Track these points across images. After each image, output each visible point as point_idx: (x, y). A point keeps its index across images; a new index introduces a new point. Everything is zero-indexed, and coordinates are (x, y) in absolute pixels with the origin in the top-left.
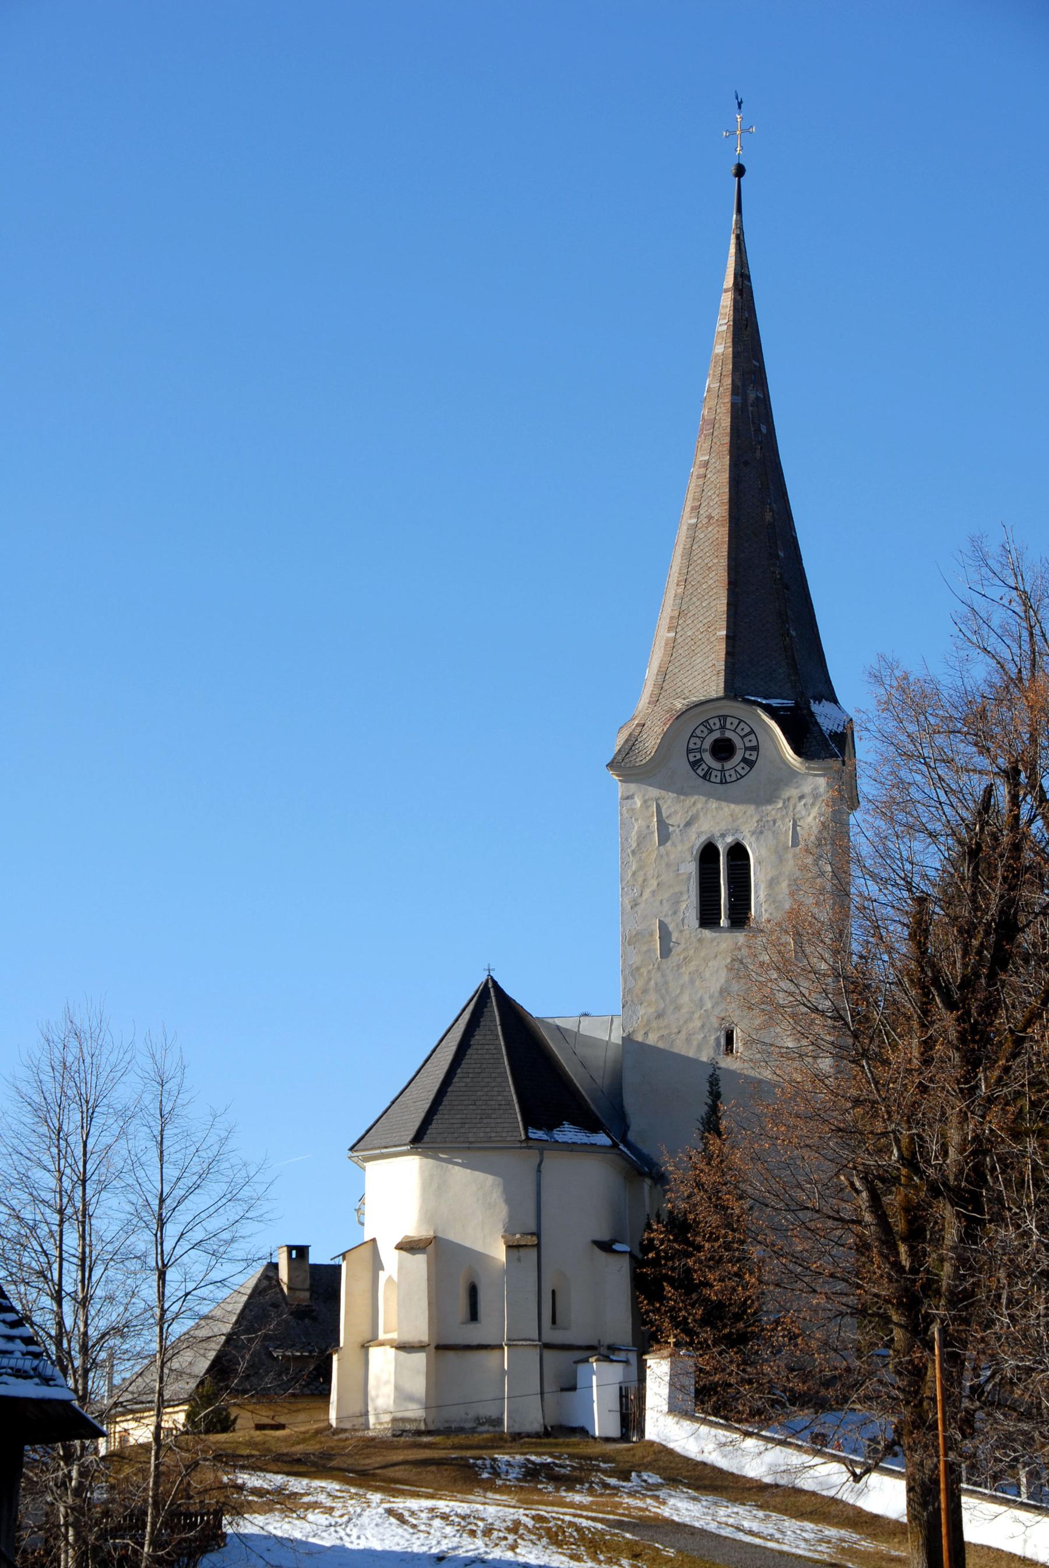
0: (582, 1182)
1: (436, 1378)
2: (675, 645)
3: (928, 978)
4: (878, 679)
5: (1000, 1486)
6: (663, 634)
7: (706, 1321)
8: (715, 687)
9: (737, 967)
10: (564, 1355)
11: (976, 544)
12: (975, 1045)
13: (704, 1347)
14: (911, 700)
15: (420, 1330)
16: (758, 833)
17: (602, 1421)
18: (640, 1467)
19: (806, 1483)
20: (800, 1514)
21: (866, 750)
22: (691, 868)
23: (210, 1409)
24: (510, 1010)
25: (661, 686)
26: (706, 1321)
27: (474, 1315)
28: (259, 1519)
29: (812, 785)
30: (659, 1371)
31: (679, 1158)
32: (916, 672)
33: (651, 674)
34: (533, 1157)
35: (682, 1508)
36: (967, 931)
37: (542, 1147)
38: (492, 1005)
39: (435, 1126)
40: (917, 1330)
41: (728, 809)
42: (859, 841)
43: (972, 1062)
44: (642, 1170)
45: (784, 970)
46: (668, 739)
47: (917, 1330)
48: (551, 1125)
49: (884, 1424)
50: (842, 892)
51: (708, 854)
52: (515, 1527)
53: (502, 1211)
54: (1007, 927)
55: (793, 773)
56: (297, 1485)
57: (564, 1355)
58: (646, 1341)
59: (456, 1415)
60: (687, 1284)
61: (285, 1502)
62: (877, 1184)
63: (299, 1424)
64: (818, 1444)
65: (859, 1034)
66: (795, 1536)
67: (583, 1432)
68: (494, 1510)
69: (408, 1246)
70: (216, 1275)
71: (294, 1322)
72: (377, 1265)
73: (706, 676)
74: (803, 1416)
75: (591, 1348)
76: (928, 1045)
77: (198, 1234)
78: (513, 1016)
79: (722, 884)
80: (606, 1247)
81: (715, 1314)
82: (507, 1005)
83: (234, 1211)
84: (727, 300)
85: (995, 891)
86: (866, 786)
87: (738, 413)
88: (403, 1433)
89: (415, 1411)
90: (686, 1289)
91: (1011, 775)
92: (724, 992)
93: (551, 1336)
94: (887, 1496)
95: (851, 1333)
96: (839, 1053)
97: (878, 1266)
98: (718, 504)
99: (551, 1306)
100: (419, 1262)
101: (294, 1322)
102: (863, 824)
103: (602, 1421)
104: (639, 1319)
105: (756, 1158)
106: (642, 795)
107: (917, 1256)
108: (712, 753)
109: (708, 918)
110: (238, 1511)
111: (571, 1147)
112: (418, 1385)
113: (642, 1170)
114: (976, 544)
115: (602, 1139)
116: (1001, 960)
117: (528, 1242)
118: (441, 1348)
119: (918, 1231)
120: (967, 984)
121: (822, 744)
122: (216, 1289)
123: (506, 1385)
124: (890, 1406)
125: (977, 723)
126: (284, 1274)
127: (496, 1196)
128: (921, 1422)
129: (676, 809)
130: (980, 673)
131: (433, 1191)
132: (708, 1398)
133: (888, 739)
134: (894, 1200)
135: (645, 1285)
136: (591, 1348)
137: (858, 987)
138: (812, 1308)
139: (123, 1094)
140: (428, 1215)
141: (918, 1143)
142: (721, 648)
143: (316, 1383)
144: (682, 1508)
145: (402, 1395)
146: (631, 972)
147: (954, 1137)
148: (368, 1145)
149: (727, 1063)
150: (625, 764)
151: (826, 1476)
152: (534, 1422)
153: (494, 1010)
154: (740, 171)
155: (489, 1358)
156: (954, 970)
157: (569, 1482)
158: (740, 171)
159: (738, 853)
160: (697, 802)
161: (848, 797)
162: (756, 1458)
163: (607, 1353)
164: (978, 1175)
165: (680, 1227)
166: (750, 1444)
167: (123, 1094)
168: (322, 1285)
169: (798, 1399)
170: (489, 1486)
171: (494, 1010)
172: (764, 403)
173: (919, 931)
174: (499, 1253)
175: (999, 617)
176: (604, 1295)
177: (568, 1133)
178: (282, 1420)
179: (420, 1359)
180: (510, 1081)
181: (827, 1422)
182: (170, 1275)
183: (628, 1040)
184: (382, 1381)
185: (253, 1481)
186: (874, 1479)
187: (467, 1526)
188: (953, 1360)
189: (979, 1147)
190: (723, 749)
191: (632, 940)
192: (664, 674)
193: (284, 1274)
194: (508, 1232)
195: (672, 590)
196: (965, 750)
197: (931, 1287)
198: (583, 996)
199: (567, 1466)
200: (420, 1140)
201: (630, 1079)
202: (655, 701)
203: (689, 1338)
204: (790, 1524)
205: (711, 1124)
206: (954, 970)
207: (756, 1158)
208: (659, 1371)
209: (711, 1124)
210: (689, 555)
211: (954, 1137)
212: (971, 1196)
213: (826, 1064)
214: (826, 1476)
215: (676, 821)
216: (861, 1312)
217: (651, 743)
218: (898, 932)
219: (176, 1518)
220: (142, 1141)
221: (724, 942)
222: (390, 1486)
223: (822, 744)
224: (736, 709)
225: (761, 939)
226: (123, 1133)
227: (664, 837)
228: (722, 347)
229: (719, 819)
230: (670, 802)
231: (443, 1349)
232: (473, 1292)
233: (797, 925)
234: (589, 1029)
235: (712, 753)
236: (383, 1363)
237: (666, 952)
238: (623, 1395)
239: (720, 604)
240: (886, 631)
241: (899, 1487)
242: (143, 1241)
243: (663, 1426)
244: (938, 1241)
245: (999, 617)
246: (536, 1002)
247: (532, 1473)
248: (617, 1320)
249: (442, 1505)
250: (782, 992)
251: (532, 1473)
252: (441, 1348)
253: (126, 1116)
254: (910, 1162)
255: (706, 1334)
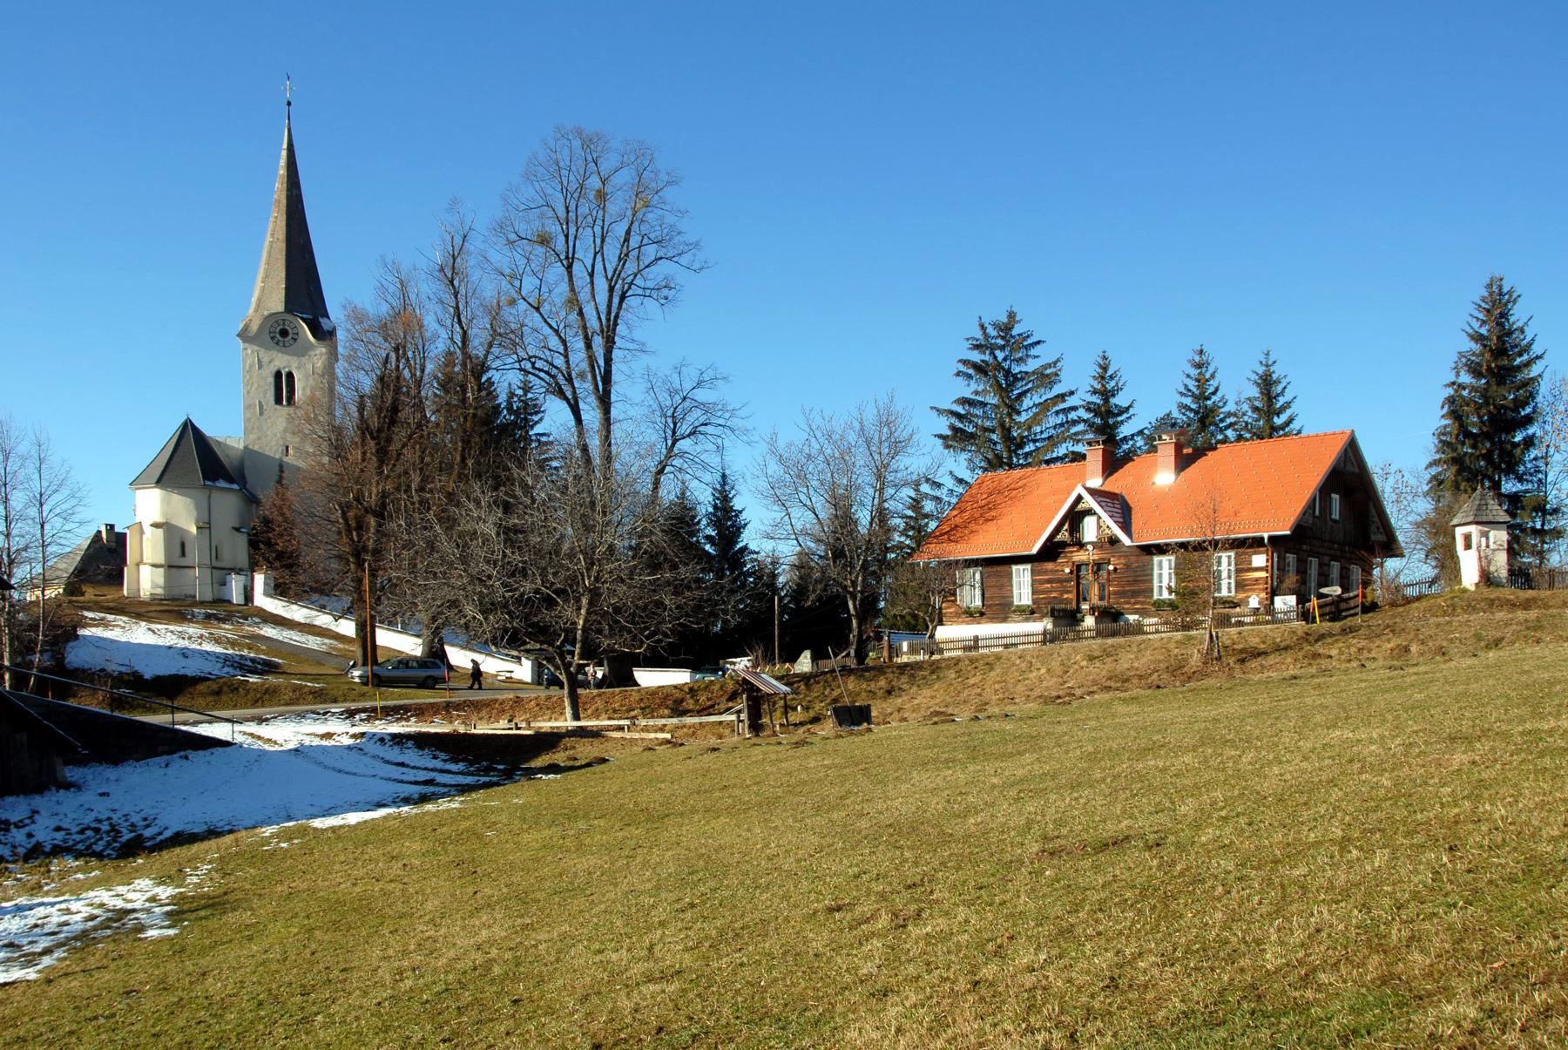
0: (227, 504)
1: (167, 578)
2: (264, 290)
3: (364, 427)
4: (344, 307)
5: (390, 624)
6: (259, 284)
7: (277, 559)
8: (281, 307)
9: (290, 419)
10: (221, 572)
11: (383, 257)
12: (382, 454)
13: (276, 569)
14: (358, 317)
15: (161, 559)
16: (298, 368)
17: (236, 597)
18: (252, 616)
19: (317, 623)
20: (314, 634)
21: (341, 335)
22: (271, 380)
23: (73, 588)
24: (198, 433)
25: (258, 305)
26: (277, 559)
27: (183, 554)
28: (94, 630)
29: (320, 351)
30: (259, 580)
31: (267, 495)
32: (360, 305)
33: (254, 299)
34: (207, 492)
35: (269, 631)
36: (379, 410)
37: (210, 488)
38: (189, 429)
39: (167, 475)
40: (360, 564)
41: (286, 357)
42: (339, 374)
43: (381, 462)
44: (251, 500)
45: (308, 420)
46: (261, 327)
47: (360, 564)
48: (214, 480)
49: (346, 601)
50: (332, 390)
51: (278, 375)
52: (201, 637)
53: (195, 513)
54: (395, 409)
55: (312, 347)
56: (110, 617)
57: (221, 572)
58: (253, 567)
59: (177, 592)
60: (269, 544)
61: (105, 624)
62: (345, 509)
63: (110, 595)
64: (322, 608)
65: (338, 450)
66: (313, 643)
67: (229, 602)
68: (192, 630)
69: (156, 525)
70: (67, 528)
71: (106, 558)
72: (142, 532)
73: (277, 303)
74: (315, 597)
75: (232, 570)
76: (364, 453)
77: (58, 511)
78: (199, 436)
79: (283, 386)
80: (237, 530)
81: (280, 556)
82: (196, 430)
83: (73, 502)
84: (284, 153)
85: (389, 397)
86: (340, 349)
87: (289, 198)
88: (155, 599)
89: (160, 591)
90: (271, 548)
91: (396, 349)
92: (285, 430)
93: (215, 564)
94: (348, 628)
95: (334, 565)
96: (330, 455)
97: (345, 540)
98: (281, 233)
99: (216, 553)
100: (160, 532)
101: (106, 558)
102: (340, 368)
103: (236, 597)
104: (251, 557)
105: (297, 495)
106: (251, 349)
107: (360, 536)
108: (278, 334)
109: (278, 401)
110: (85, 626)
111: (223, 489)
112: (161, 581)
113: (251, 500)
114: (383, 257)
115: (235, 486)
116: (393, 422)
117: (205, 526)
118: (170, 567)
119: (361, 526)
120: (380, 430)
121: (324, 334)
122: (74, 540)
123: (198, 583)
124: (349, 593)
125: (384, 328)
126: (104, 535)
127: (192, 507)
128: (361, 600)
129: (266, 356)
130: (384, 309)
131: (166, 503)
132: (279, 590)
133: (348, 331)
134: (351, 514)
135: (253, 544)
136: (232, 570)
137: (338, 431)
138: (319, 556)
139: (23, 448)
140: (164, 514)
141: (360, 492)
142: (283, 292)
143: (116, 578)
144: (269, 631)
145: (155, 586)
146: (247, 420)
147: (374, 491)
148: (137, 483)
149: (286, 459)
150: (244, 335)
151: (324, 620)
152: (209, 597)
153: (189, 431)
154: (289, 104)
155: (190, 572)
156: (375, 423)
157: (224, 621)
158: (289, 104)
159: (290, 376)
160: (274, 353)
161: (333, 355)
162: (298, 613)
163: (239, 571)
164: (384, 506)
165: (267, 522)
166: (294, 607)
167: (23, 448)
168: (120, 539)
169: (314, 590)
170: (190, 621)
171: (189, 431)
172: (300, 196)
173: (361, 407)
174: (194, 530)
175: (392, 289)
176: (236, 550)
177: (222, 484)
178: (216, 814)
179: (161, 570)
180: (195, 460)
181: (324, 600)
182: (47, 527)
183: (246, 447)
184: (146, 579)
185: (90, 615)
186: (342, 621)
187: (181, 635)
188: (373, 575)
189: (384, 495)
190: (284, 333)
191: (248, 407)
192: (259, 300)
193: (104, 535)
194: (197, 522)
195: (263, 267)
196: (379, 339)
197: (365, 549)
198: (228, 430)
199: (223, 614)
200: (159, 482)
201: (247, 463)
202: (256, 310)
203: (271, 567)
204: (310, 637)
205: (280, 481)
206: (375, 423)
207: (297, 495)
208: (259, 580)
209: (280, 481)
210: (270, 253)
211: (374, 491)
212: (380, 514)
213: (326, 459)
214: (324, 620)
215: (265, 360)
216: (339, 557)
217: (254, 328)
218: (353, 410)
219: (53, 626)
220: (31, 468)
221: (284, 410)
222: (149, 619)
223: (324, 334)
224: (289, 317)
225: (300, 413)
226: (22, 466)
227: (260, 367)
228: (282, 172)
229: (283, 361)
230: (262, 352)
231: (170, 567)
232: (183, 545)
233: (312, 400)
234: (229, 442)
235: (278, 334)
236: (146, 571)
237: (261, 413)
238: (245, 588)
239: (283, 275)
240: (346, 289)
241: (353, 625)
242: (33, 512)
243: (262, 600)
244: (368, 529)
245: (392, 289)
246: (208, 430)
247: (208, 617)
248: (242, 558)
249: (171, 628)
250: (307, 428)
251: (208, 617)
252: (170, 567)
253: (24, 458)
254: (357, 499)
255: (277, 564)
